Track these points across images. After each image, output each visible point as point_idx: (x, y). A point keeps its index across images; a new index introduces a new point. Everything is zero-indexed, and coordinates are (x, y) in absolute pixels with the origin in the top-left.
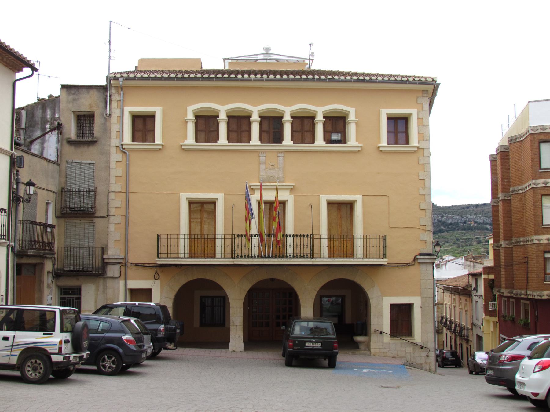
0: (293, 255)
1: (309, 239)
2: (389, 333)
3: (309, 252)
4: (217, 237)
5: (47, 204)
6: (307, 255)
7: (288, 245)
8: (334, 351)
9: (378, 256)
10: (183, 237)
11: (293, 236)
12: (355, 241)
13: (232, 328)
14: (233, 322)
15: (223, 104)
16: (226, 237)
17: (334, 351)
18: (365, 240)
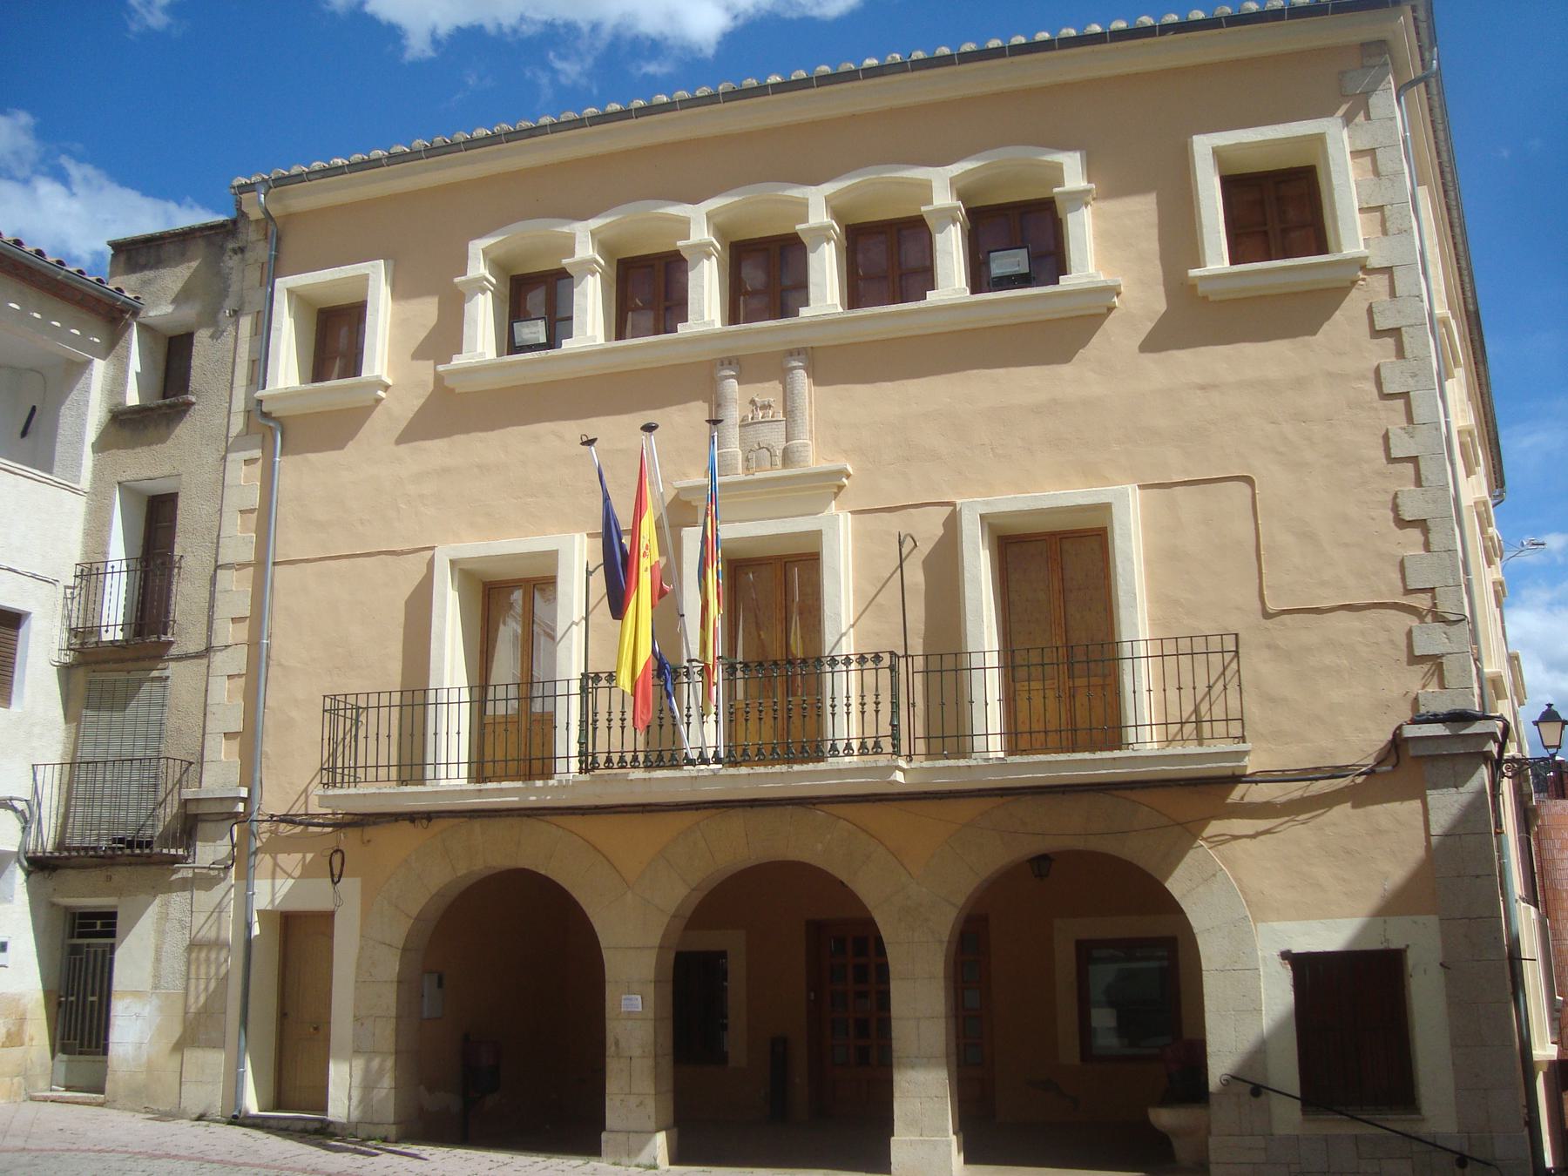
0: (863, 746)
1: (885, 675)
2: (1294, 1087)
3: (886, 729)
4: (432, 699)
5: (589, 573)
6: (877, 745)
7: (841, 702)
8: (1549, 1162)
9: (383, 772)
10: (1142, 649)
11: (862, 659)
12: (1126, 666)
13: (612, 1066)
14: (617, 1043)
15: (695, 200)
16: (1170, 648)
17: (1549, 1162)
18: (935, 677)
